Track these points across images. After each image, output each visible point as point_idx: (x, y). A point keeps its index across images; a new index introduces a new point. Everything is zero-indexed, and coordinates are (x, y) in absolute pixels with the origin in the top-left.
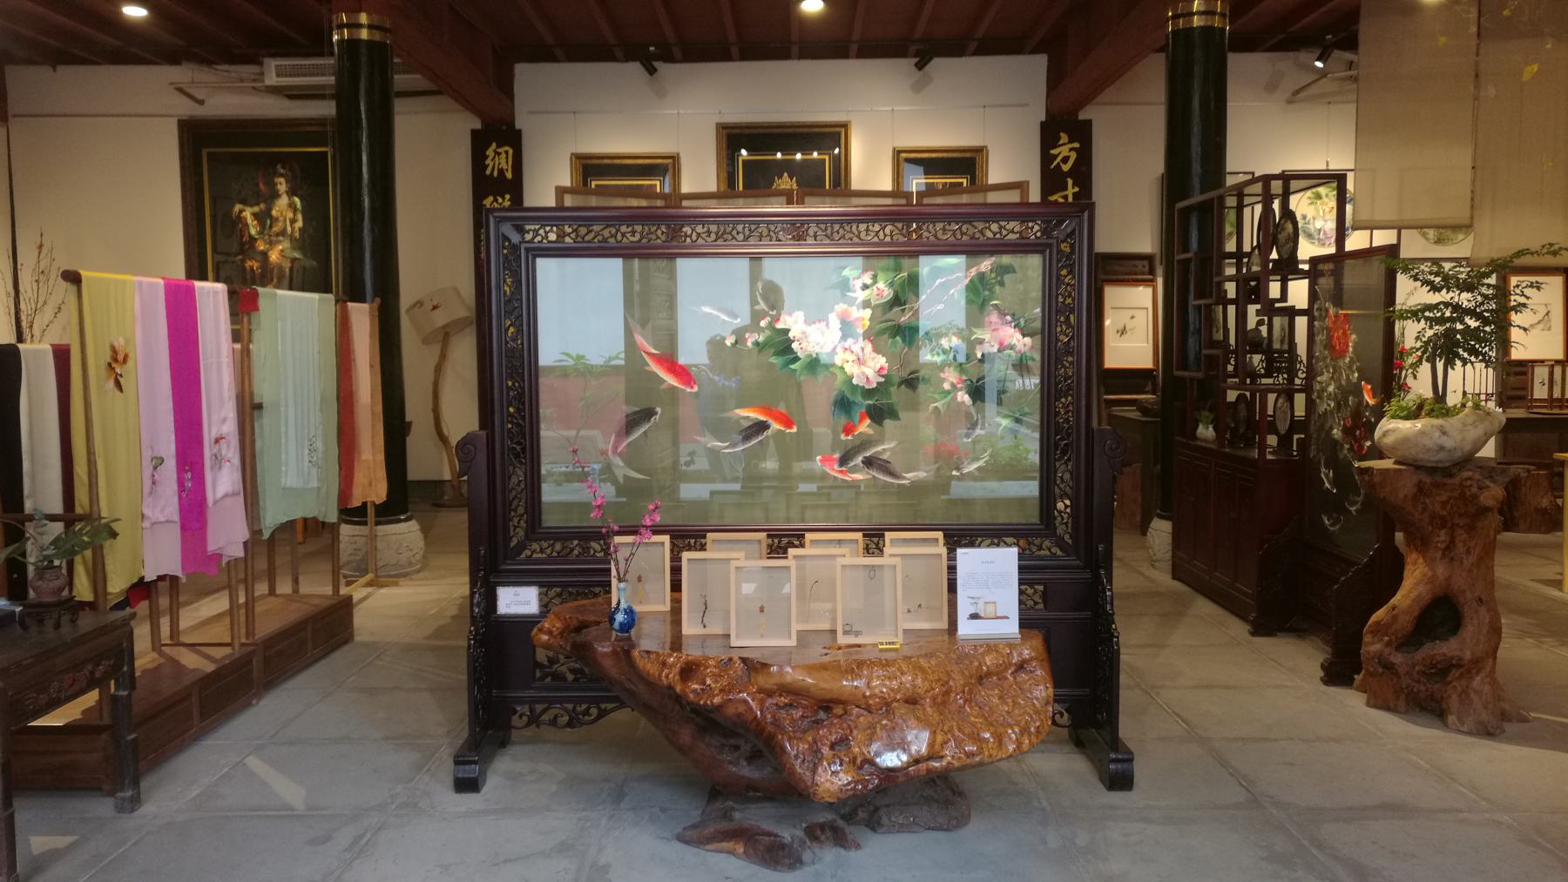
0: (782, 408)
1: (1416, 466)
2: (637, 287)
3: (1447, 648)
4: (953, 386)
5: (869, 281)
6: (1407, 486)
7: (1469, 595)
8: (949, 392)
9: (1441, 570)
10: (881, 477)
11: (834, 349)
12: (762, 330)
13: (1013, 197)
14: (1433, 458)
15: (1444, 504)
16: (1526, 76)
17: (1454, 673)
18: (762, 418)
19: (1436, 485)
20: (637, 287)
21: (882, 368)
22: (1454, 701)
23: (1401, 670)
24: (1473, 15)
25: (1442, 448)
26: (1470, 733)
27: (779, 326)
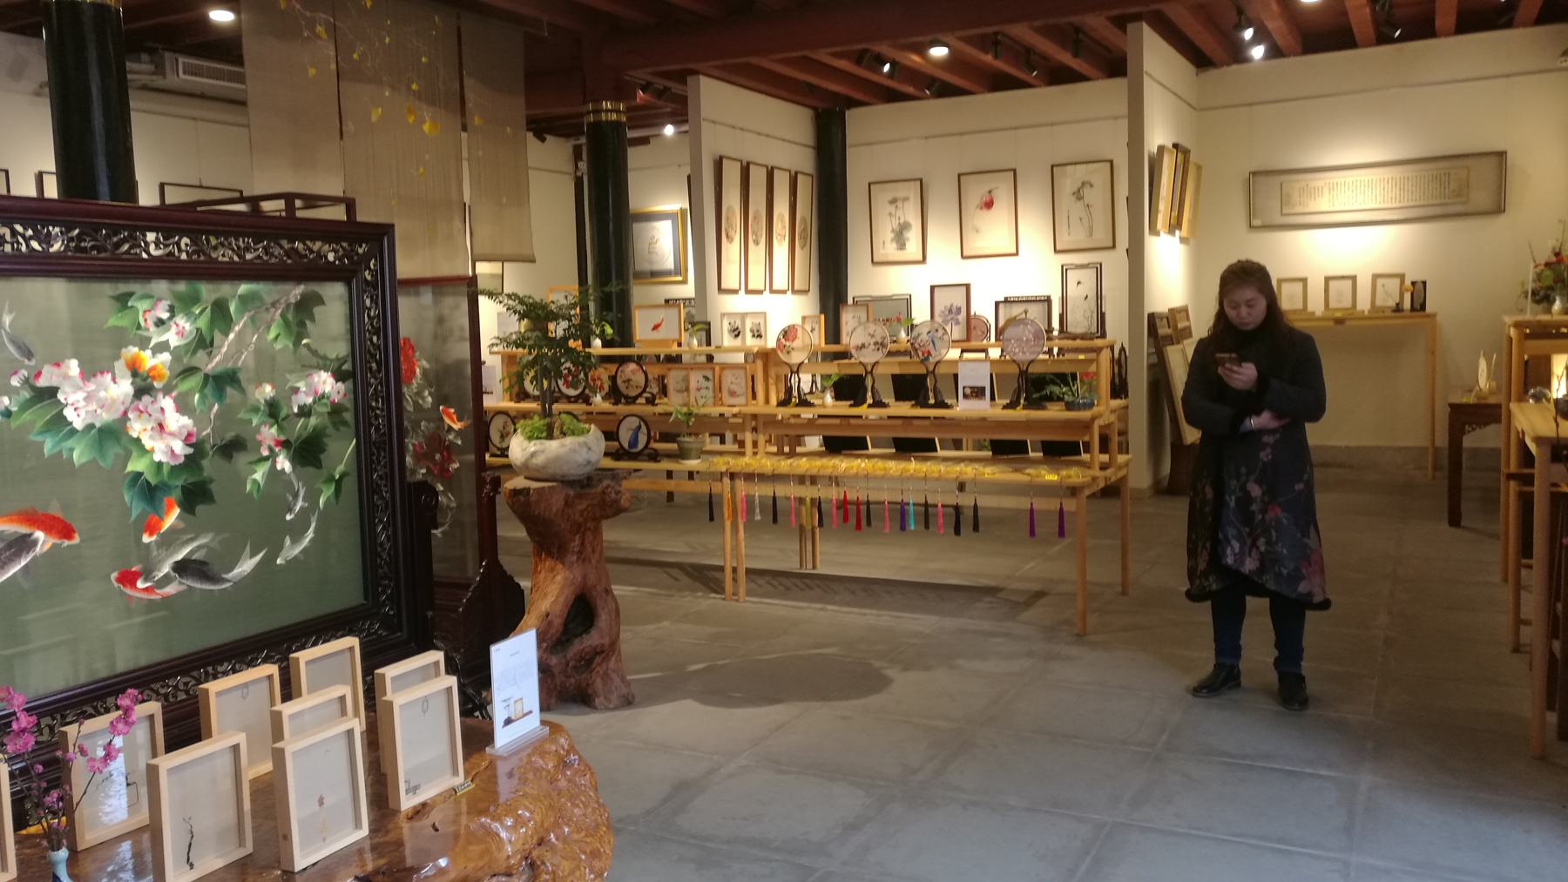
0: (55, 510)
1: (566, 482)
2: (1082, 357)
3: (593, 639)
4: (271, 449)
5: (165, 316)
6: (557, 502)
7: (599, 588)
8: (266, 459)
9: (577, 573)
10: (198, 585)
11: (125, 413)
12: (15, 391)
13: (338, 213)
14: (576, 472)
15: (582, 512)
16: (374, 118)
17: (598, 659)
18: (24, 530)
19: (579, 496)
20: (1082, 357)
21: (190, 435)
22: (599, 683)
23: (556, 671)
24: (333, 53)
25: (589, 462)
26: (616, 708)
27: (42, 382)
